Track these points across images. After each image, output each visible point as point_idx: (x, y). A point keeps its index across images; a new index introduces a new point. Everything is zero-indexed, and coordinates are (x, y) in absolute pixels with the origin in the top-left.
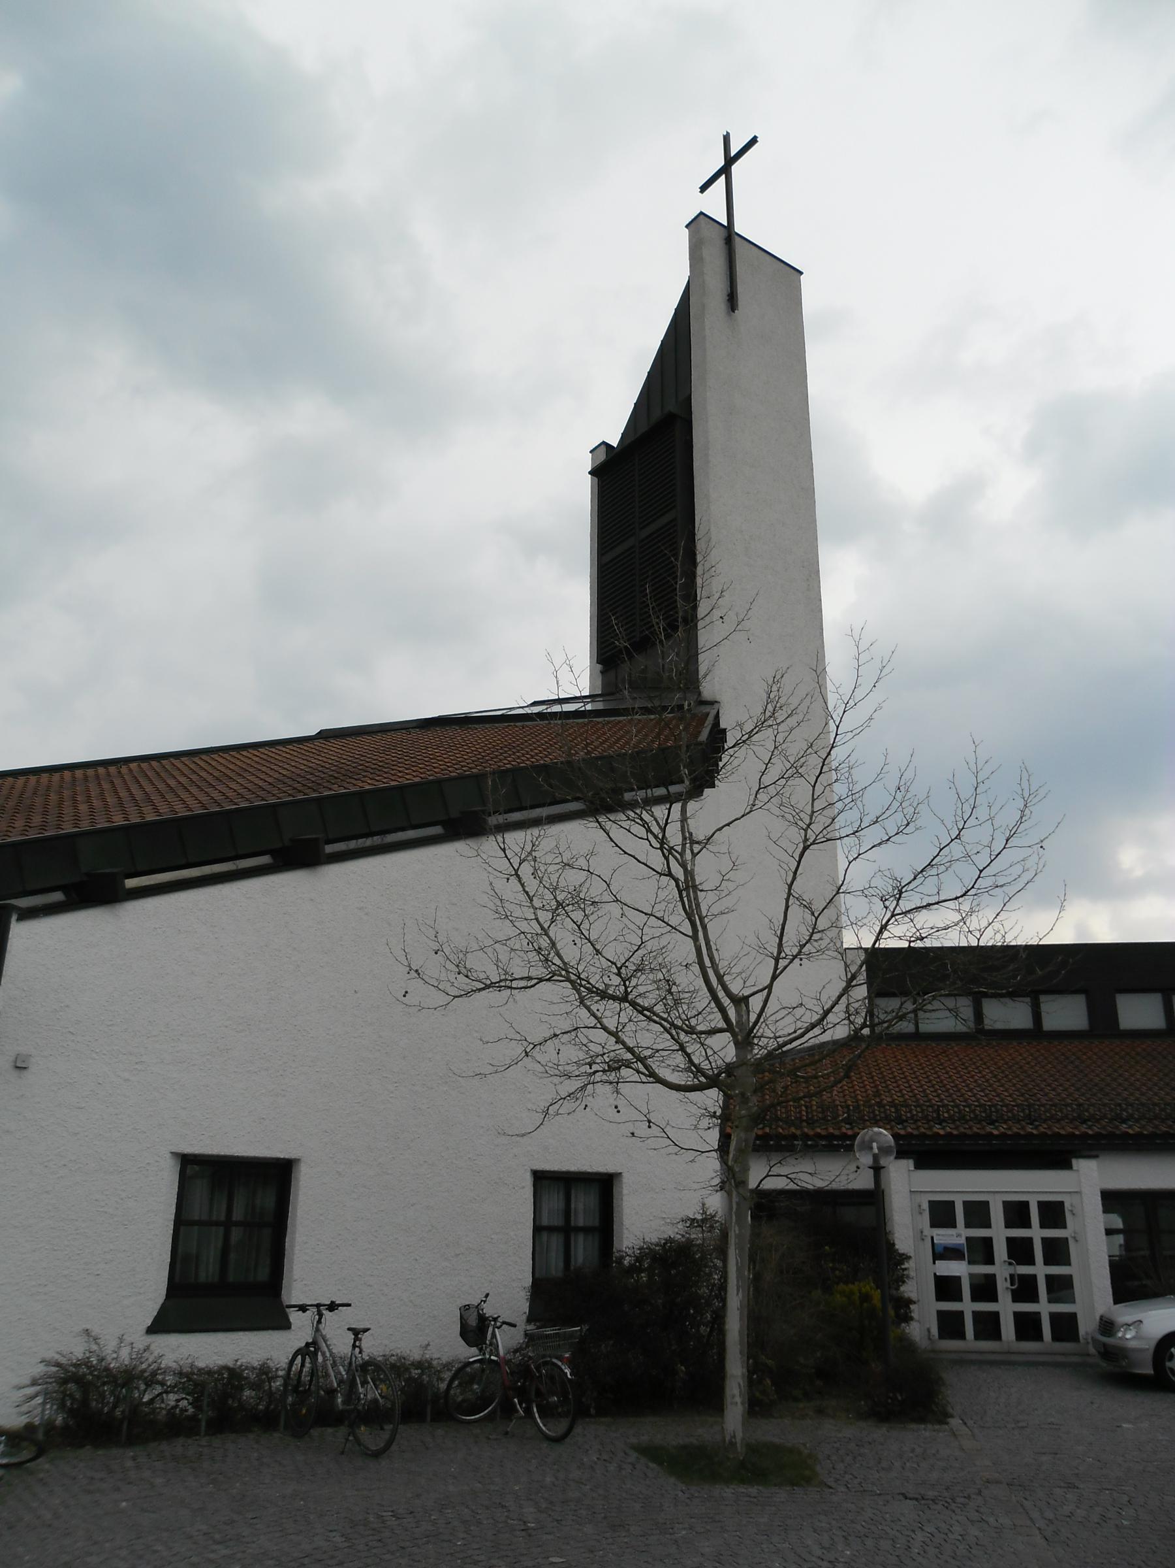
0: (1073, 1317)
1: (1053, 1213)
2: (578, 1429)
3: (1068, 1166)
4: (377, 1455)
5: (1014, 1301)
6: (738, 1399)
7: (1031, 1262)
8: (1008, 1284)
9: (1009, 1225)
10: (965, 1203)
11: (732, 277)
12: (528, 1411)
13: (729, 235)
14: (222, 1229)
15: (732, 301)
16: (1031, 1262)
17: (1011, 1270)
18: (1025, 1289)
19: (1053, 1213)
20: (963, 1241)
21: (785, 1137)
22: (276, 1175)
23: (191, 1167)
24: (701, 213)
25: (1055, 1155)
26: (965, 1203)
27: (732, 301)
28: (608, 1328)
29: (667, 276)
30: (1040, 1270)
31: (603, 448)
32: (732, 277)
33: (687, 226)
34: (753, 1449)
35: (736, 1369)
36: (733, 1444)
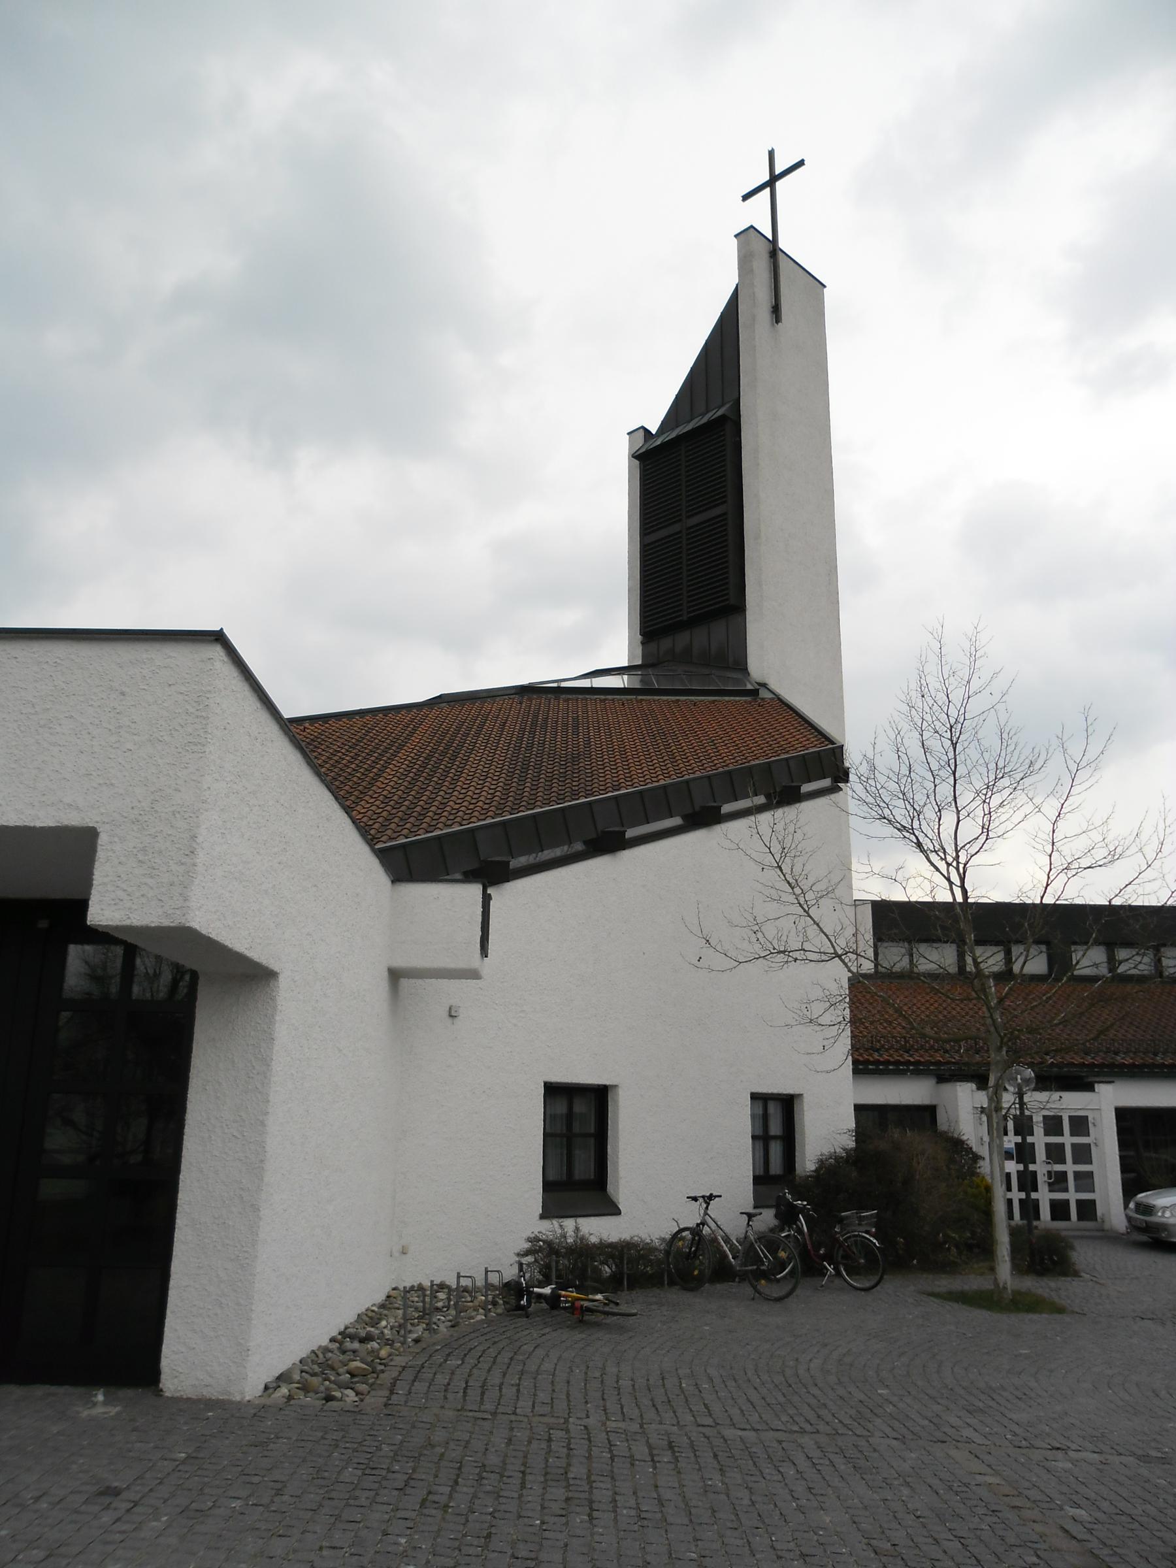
0: (1093, 1202)
1: (1080, 1125)
2: (798, 1291)
3: (1090, 1088)
4: (779, 1299)
5: (1050, 1191)
6: (1007, 1258)
7: (1063, 1162)
8: (1046, 1178)
9: (1047, 1133)
10: (1070, 1117)
11: (772, 287)
12: (838, 1273)
13: (774, 251)
14: (592, 1141)
15: (776, 310)
16: (1063, 1162)
17: (1049, 1167)
18: (1058, 1181)
19: (1080, 1125)
20: (1013, 1146)
21: (872, 1063)
22: (600, 1096)
23: (552, 1091)
24: (752, 227)
25: (1079, 1082)
26: (1070, 1117)
27: (776, 310)
28: (859, 1214)
29: (719, 279)
30: (1070, 1167)
31: (642, 432)
32: (772, 287)
33: (736, 236)
34: (1016, 1293)
35: (1003, 1239)
36: (1005, 1288)
